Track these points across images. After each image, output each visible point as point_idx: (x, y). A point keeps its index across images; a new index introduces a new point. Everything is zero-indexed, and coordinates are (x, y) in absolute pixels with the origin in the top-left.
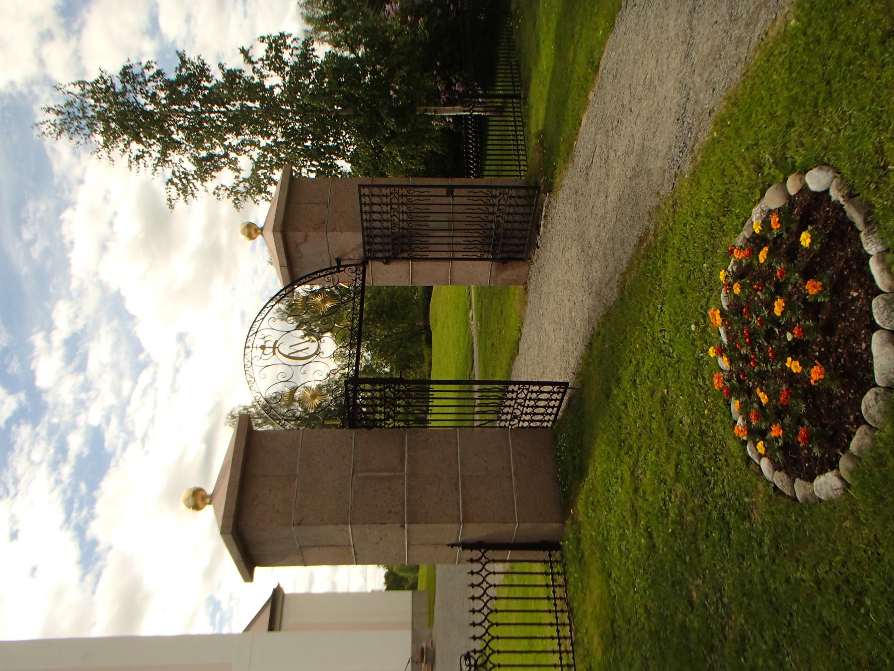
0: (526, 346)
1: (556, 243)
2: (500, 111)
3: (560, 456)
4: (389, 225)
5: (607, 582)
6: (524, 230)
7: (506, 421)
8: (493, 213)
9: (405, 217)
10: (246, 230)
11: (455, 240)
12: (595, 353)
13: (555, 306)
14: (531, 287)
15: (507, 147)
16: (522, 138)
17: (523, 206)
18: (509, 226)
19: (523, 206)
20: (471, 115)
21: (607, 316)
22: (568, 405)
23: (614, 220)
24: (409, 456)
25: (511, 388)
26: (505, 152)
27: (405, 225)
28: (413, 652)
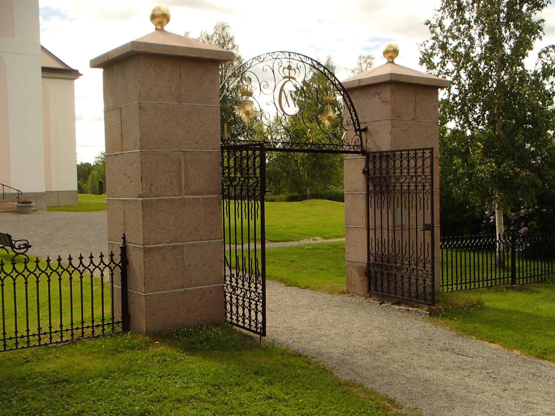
0: (294, 293)
1: (385, 321)
2: (501, 265)
3: (202, 330)
4: (398, 174)
5: (100, 375)
6: (396, 291)
7: (231, 281)
8: (410, 265)
9: (405, 188)
10: (391, 49)
11: (385, 231)
12: (292, 360)
13: (331, 321)
14: (345, 298)
15: (468, 272)
16: (477, 286)
17: (417, 290)
18: (399, 278)
19: (417, 290)
20: (496, 240)
21: (325, 371)
22: (246, 336)
23: (408, 375)
24: (199, 199)
26: (463, 270)
27: (398, 188)
28: (26, 194)
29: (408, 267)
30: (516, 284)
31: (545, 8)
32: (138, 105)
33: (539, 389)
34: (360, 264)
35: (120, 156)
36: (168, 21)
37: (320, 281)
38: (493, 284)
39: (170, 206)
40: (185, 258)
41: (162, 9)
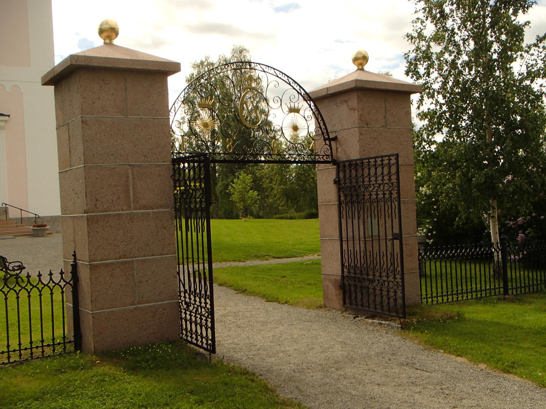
1: (353, 335)
4: (367, 183)
7: (185, 297)
8: (381, 276)
9: (374, 197)
10: (360, 56)
14: (321, 312)
17: (389, 303)
18: (371, 291)
21: (266, 389)
22: (198, 354)
23: (354, 393)
24: (149, 213)
25: (208, 301)
26: (459, 281)
27: (367, 197)
28: (44, 217)
29: (379, 279)
30: (509, 295)
31: (530, 9)
32: (80, 119)
33: (493, 405)
34: (335, 277)
35: (69, 172)
36: (117, 34)
37: (302, 296)
38: (483, 295)
39: (118, 221)
40: (135, 274)
41: (110, 23)
